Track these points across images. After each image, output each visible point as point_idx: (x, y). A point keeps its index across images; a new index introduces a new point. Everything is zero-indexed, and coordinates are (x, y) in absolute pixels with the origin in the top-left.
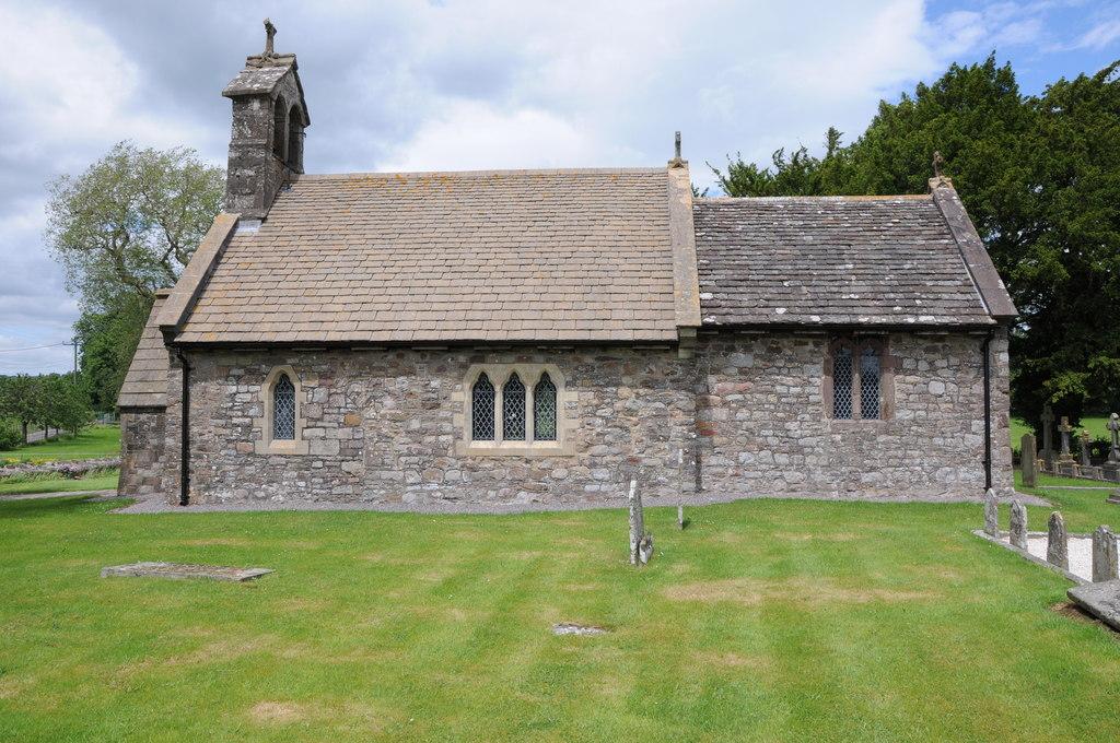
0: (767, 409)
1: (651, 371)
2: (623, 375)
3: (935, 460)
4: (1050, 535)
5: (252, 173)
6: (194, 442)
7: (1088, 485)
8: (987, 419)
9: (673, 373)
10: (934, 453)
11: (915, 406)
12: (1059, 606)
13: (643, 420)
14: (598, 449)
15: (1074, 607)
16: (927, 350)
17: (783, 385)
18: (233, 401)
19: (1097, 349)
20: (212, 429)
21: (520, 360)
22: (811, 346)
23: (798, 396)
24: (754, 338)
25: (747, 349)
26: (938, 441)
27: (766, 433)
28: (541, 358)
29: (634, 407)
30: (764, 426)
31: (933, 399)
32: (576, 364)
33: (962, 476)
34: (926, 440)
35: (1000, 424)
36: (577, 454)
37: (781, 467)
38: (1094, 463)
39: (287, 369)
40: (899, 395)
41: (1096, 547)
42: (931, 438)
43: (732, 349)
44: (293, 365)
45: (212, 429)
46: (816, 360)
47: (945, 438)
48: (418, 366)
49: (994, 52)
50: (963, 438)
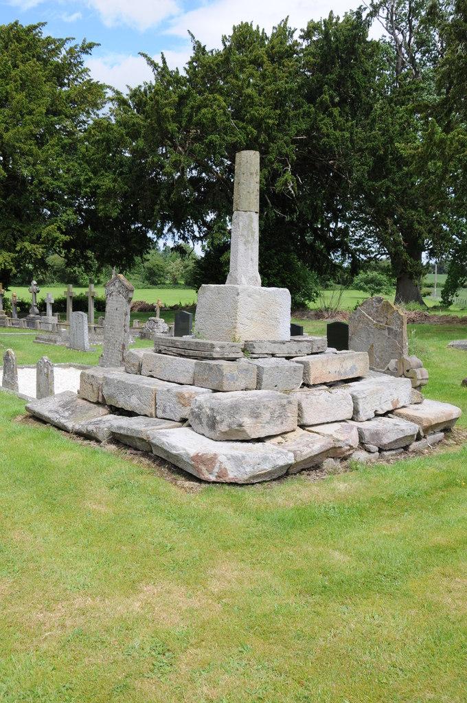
4: (5, 366)
7: (18, 332)
12: (19, 418)
15: (30, 417)
19: (22, 236)
38: (20, 317)
41: (39, 373)
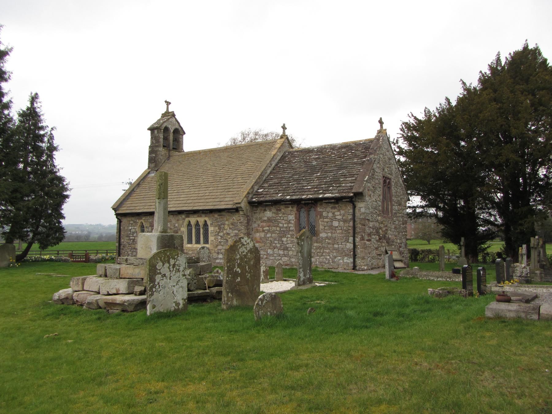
0: (276, 233)
1: (233, 219)
2: (226, 221)
3: (335, 254)
5: (154, 155)
6: (122, 245)
8: (354, 237)
9: (240, 220)
10: (334, 251)
11: (327, 231)
13: (232, 237)
14: (220, 247)
16: (332, 208)
17: (281, 223)
18: (131, 232)
20: (126, 240)
21: (198, 216)
22: (290, 208)
23: (286, 228)
24: (267, 205)
25: (270, 210)
26: (336, 246)
27: (276, 242)
28: (203, 215)
29: (229, 232)
30: (275, 239)
31: (334, 228)
32: (213, 217)
33: (345, 261)
34: (331, 246)
35: (360, 239)
36: (214, 249)
37: (281, 255)
39: (142, 221)
40: (321, 227)
42: (333, 244)
43: (265, 210)
44: (144, 220)
45: (126, 240)
46: (292, 214)
47: (338, 245)
48: (172, 219)
49: (526, 40)
50: (346, 245)
